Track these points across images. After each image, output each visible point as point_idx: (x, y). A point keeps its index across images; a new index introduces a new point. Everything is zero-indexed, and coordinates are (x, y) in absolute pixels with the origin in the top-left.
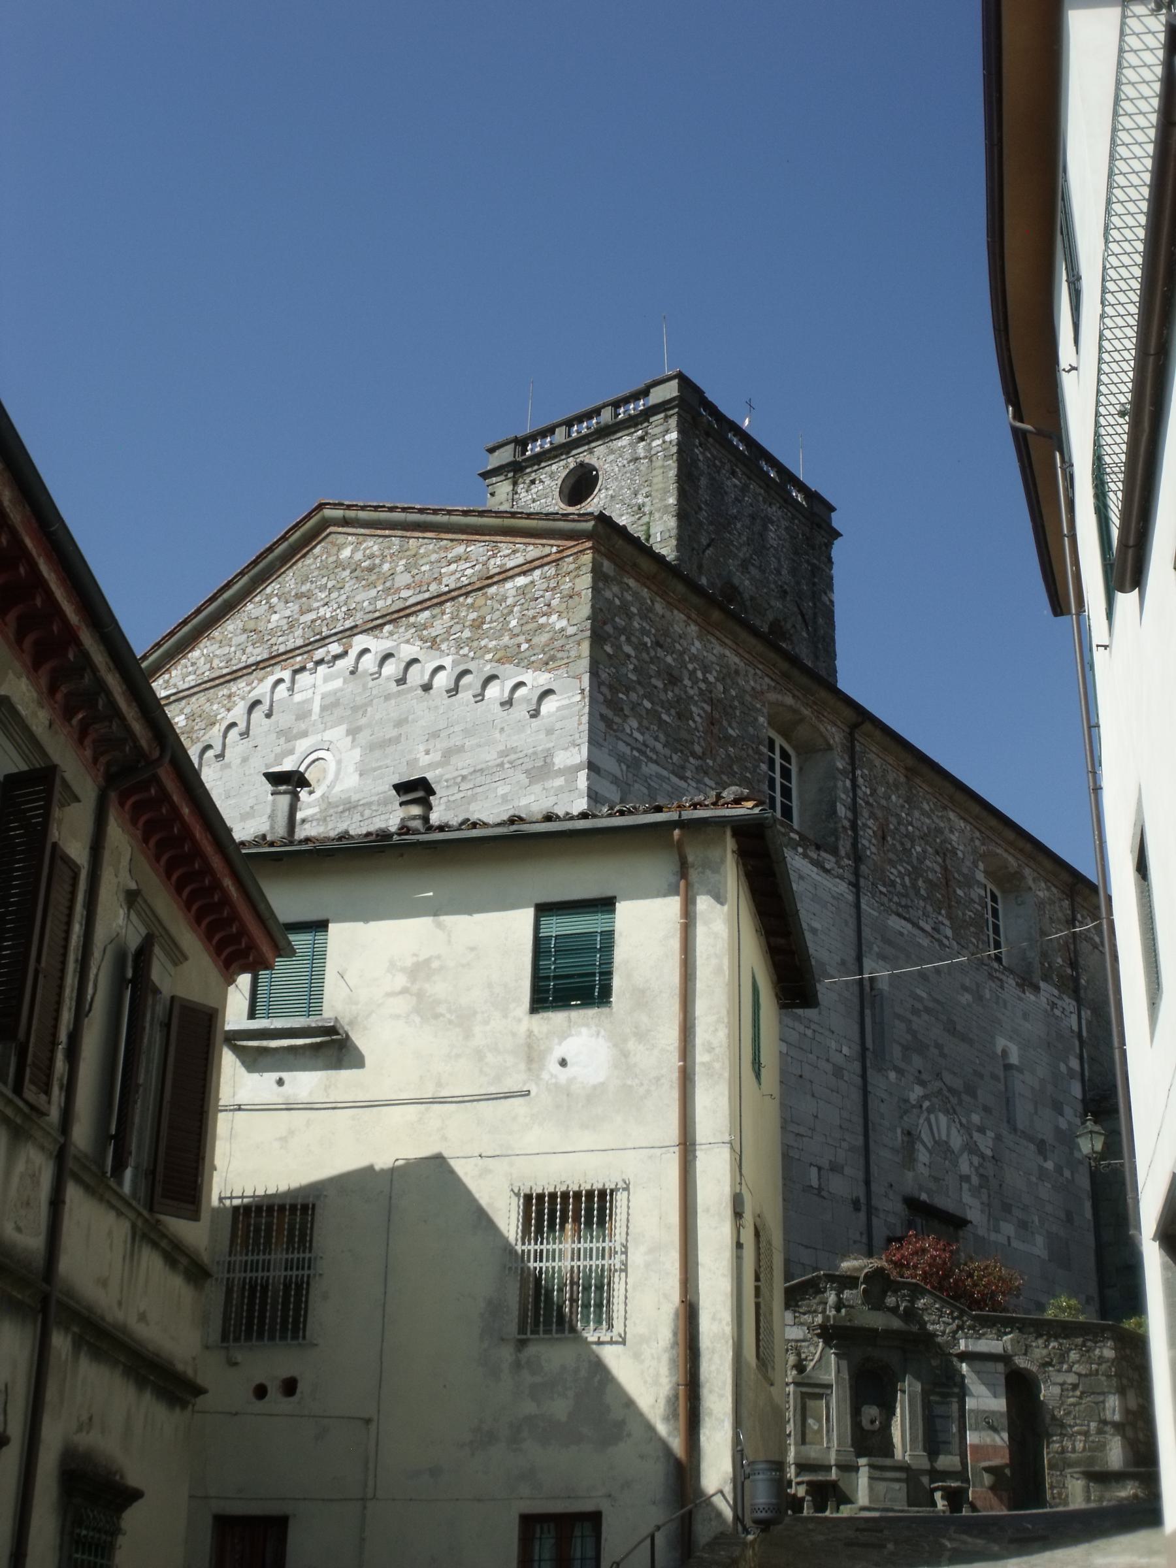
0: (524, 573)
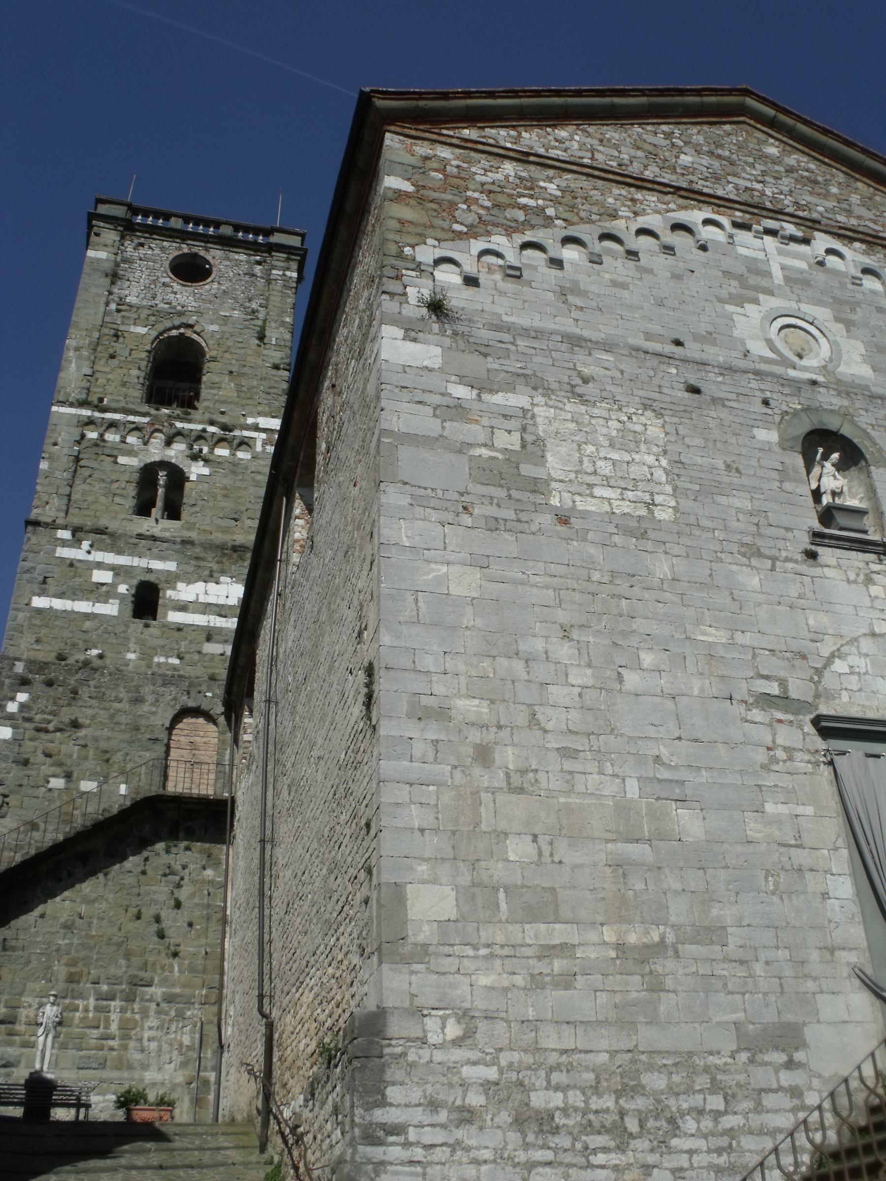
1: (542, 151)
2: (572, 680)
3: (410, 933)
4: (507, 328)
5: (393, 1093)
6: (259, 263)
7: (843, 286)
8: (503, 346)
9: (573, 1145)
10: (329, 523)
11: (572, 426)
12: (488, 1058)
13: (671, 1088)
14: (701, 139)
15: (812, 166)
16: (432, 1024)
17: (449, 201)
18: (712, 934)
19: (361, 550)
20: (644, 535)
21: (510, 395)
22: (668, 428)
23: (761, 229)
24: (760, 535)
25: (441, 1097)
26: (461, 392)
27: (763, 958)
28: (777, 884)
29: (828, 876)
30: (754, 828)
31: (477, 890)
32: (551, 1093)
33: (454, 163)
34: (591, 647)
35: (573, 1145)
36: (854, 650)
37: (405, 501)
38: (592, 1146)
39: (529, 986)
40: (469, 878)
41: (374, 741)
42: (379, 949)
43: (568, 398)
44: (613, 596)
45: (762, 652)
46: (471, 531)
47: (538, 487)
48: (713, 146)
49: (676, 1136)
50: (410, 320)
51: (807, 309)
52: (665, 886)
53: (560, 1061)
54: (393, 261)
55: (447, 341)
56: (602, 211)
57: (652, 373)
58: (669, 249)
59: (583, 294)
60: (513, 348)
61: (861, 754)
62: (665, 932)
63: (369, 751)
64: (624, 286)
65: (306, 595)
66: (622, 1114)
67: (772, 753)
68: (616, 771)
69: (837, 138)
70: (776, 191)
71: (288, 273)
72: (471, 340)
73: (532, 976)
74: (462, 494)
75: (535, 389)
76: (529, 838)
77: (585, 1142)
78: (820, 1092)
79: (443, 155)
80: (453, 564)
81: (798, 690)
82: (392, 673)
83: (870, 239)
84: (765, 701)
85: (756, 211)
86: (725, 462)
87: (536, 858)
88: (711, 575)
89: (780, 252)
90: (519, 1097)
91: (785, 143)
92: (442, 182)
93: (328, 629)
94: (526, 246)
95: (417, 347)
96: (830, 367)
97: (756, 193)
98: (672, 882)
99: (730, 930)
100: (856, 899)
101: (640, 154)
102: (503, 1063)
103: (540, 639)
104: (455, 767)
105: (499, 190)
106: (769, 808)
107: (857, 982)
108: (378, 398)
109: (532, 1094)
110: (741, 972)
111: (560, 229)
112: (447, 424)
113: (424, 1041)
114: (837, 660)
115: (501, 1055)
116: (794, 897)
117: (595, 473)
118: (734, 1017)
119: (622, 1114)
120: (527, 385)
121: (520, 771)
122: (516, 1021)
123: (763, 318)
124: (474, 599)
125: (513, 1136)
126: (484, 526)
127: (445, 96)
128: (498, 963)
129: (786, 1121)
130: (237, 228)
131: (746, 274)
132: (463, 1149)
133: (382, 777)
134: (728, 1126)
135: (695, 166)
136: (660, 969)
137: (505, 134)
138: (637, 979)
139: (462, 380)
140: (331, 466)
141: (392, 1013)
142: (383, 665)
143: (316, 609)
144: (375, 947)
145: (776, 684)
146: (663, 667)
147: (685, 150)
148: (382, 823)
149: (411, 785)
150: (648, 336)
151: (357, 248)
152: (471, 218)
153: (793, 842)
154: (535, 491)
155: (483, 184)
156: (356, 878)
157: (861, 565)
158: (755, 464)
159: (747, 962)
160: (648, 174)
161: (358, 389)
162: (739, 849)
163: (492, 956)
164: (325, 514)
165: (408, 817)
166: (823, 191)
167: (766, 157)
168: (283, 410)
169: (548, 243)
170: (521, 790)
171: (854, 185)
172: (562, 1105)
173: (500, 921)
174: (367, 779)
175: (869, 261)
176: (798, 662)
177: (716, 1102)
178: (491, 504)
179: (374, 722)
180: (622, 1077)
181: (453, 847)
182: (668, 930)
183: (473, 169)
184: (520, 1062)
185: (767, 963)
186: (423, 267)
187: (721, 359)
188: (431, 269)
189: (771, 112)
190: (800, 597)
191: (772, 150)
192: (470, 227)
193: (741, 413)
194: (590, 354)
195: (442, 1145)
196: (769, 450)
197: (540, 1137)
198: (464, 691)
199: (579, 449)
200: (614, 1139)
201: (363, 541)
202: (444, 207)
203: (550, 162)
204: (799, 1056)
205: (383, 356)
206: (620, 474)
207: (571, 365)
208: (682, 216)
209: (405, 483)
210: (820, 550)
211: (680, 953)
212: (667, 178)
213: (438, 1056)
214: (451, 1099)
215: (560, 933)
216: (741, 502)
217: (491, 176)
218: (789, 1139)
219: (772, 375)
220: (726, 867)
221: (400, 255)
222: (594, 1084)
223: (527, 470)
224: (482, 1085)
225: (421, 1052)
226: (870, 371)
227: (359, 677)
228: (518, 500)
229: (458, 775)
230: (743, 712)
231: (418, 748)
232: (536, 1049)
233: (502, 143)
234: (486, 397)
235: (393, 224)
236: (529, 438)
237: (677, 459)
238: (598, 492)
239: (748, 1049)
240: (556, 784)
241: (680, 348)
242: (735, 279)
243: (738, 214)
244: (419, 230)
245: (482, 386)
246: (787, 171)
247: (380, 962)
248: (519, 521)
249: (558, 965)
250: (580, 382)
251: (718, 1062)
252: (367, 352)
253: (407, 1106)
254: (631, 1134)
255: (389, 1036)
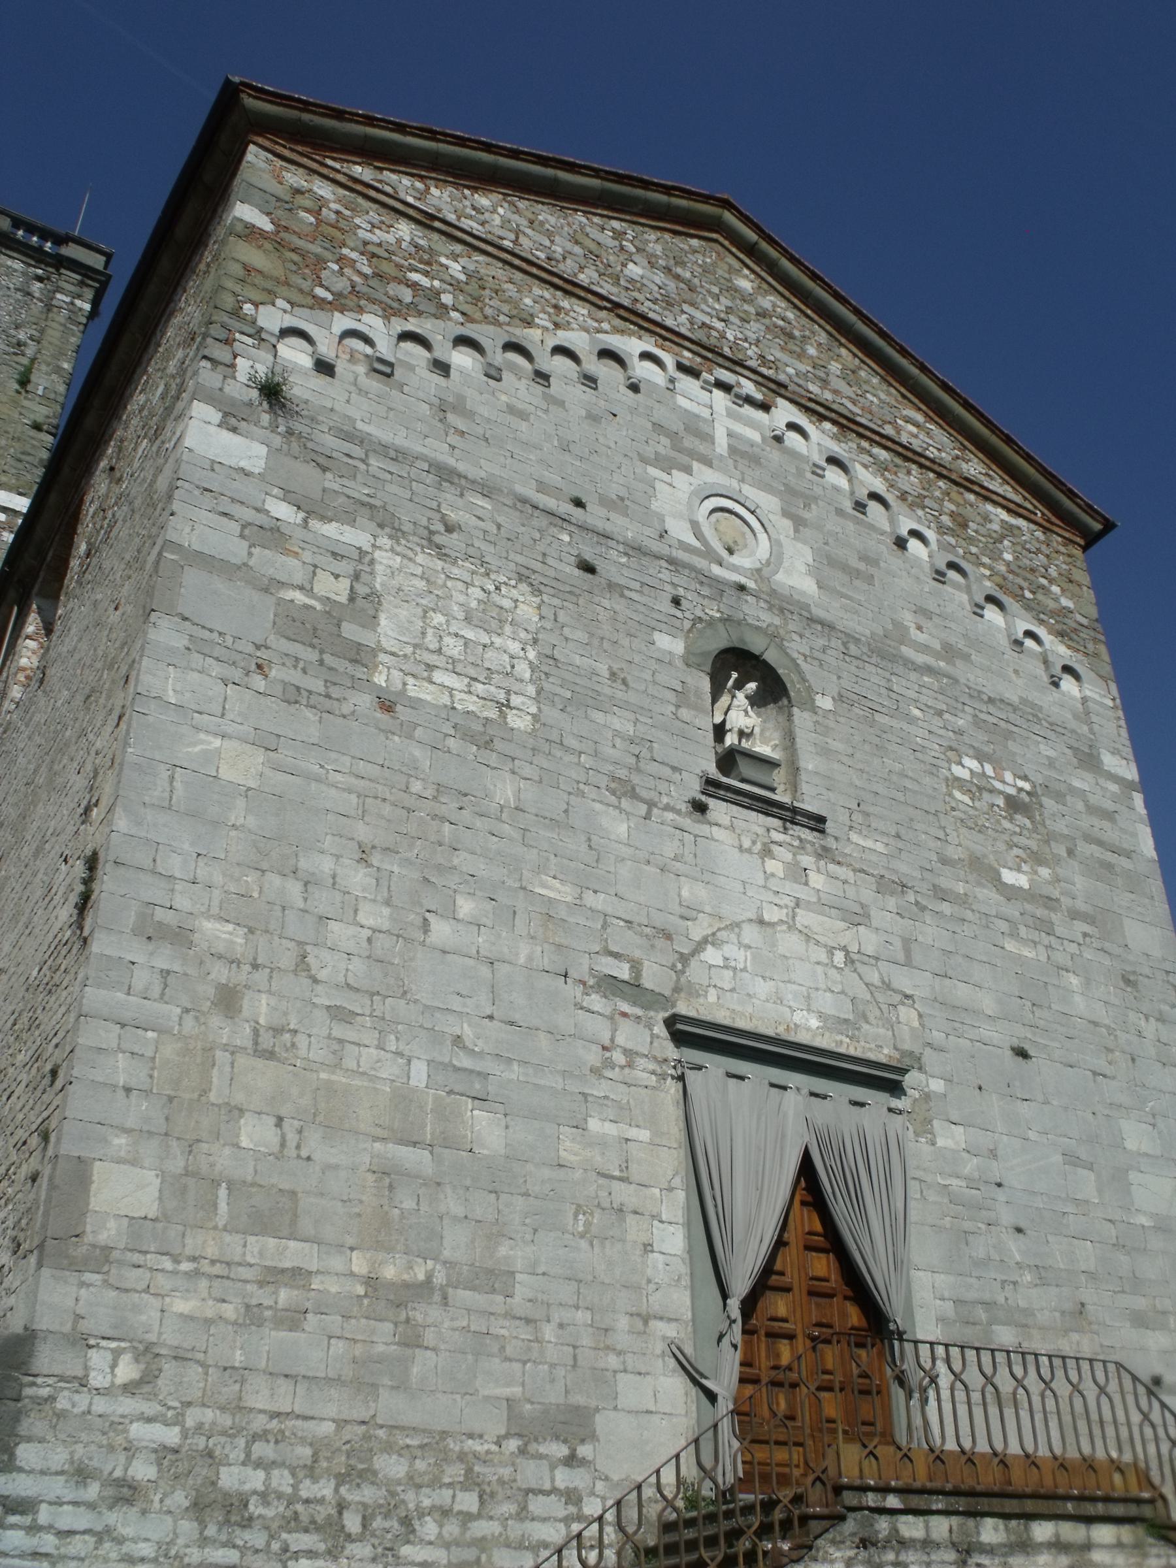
0: (1009, 511)
1: (452, 217)
2: (361, 918)
3: (89, 1228)
4: (360, 439)
5: (26, 1454)
6: (40, 279)
7: (800, 473)
8: (350, 461)
9: (268, 1544)
10: (71, 653)
11: (422, 584)
12: (170, 1414)
13: (411, 1478)
14: (658, 249)
15: (790, 315)
16: (98, 1359)
17: (316, 255)
18: (494, 1279)
19: (109, 697)
20: (488, 744)
21: (346, 528)
22: (545, 611)
23: (712, 379)
24: (638, 770)
25: (95, 1463)
26: (282, 511)
27: (556, 1317)
28: (588, 1224)
29: (656, 1223)
30: (569, 1148)
31: (191, 1182)
32: (249, 1471)
33: (333, 206)
34: (394, 879)
35: (268, 1544)
36: (733, 937)
37: (180, 642)
38: (293, 1548)
39: (241, 1321)
40: (182, 1164)
41: (82, 959)
42: (41, 1246)
43: (423, 547)
44: (435, 817)
45: (616, 921)
46: (262, 699)
47: (361, 655)
48: (672, 262)
49: (408, 1542)
50: (233, 402)
51: (750, 492)
52: (442, 1209)
53: (268, 1427)
54: (225, 318)
55: (277, 441)
56: (515, 312)
57: (538, 536)
58: (590, 380)
59: (470, 415)
60: (363, 467)
61: (721, 1072)
62: (433, 1270)
63: (73, 971)
64: (523, 416)
65: (21, 746)
66: (341, 1507)
67: (608, 1054)
68: (401, 1048)
69: (827, 287)
70: (740, 336)
71: (78, 302)
72: (310, 445)
73: (248, 1307)
74: (258, 647)
75: (381, 526)
76: (272, 1121)
77: (285, 1542)
78: (604, 1499)
79: (321, 192)
80: (230, 737)
81: (654, 977)
82: (122, 870)
83: (845, 422)
84: (610, 985)
85: (710, 355)
86: (610, 668)
87: (276, 1149)
88: (566, 811)
89: (730, 414)
90: (204, 1472)
91: (763, 279)
92: (311, 229)
93: (44, 796)
94: (406, 336)
95: (236, 439)
96: (765, 573)
97: (714, 333)
98: (452, 1204)
99: (519, 1277)
100: (686, 1256)
101: (577, 250)
102: (190, 1423)
103: (329, 858)
104: (187, 1011)
105: (386, 255)
106: (594, 1125)
107: (672, 1362)
108: (170, 497)
109: (223, 1469)
110: (525, 1333)
111: (454, 325)
112: (256, 551)
113: (83, 1382)
114: (709, 947)
115: (190, 1412)
116: (608, 1243)
117: (439, 651)
118: (507, 1391)
119: (341, 1507)
120: (371, 519)
121: (274, 1029)
122: (216, 1366)
123: (692, 493)
124: (249, 789)
125: (187, 1527)
126: (280, 694)
127: (339, 115)
128: (203, 1284)
129: (554, 1534)
130: (17, 223)
131: (682, 433)
132: (113, 1540)
133: (85, 1010)
134: (479, 1535)
135: (645, 281)
136: (419, 1317)
137: (409, 184)
138: (388, 1327)
139: (288, 496)
140: (88, 577)
141: (45, 1339)
142: (111, 858)
143: (32, 767)
144: (36, 1242)
145: (626, 966)
146: (484, 920)
147: (636, 258)
148: (75, 1073)
149: (123, 1026)
150: (542, 487)
151: (180, 290)
152: (341, 285)
153: (617, 1173)
154: (356, 661)
155: (366, 243)
156: (25, 1143)
157: (761, 831)
158: (649, 678)
159: (535, 1321)
160: (583, 278)
161: (144, 480)
162: (547, 1173)
163: (197, 1273)
164: (67, 640)
165: (112, 1067)
166: (798, 350)
167: (736, 291)
168: (35, 487)
169: (436, 339)
170: (270, 1055)
171: (836, 350)
172: (260, 1487)
173: (215, 1228)
174: (63, 1009)
175: (838, 449)
176: (660, 943)
177: (468, 1501)
178: (295, 667)
179: (85, 934)
180: (348, 1457)
181: (167, 1119)
182: (438, 1267)
183: (357, 221)
184: (214, 1423)
185: (561, 1326)
186: (264, 336)
187: (630, 535)
188: (273, 340)
189: (752, 236)
190: (676, 858)
191: (745, 283)
192: (338, 295)
193: (642, 609)
194: (462, 495)
195: (84, 1532)
196: (670, 663)
197: (225, 1530)
198: (215, 910)
199: (425, 617)
200: (324, 1541)
201: (114, 684)
202: (309, 261)
203: (459, 234)
204: (584, 1451)
205: (188, 442)
206: (471, 659)
207: (434, 505)
208: (616, 342)
209: (185, 619)
210: (712, 803)
211: (450, 1300)
212: (606, 288)
213: (101, 1405)
214: (109, 1468)
215: (295, 1253)
216: (621, 723)
217: (379, 236)
218: (555, 1557)
219: (692, 568)
220: (526, 1194)
221: (236, 313)
222: (309, 1463)
223: (350, 631)
224: (155, 1451)
225: (76, 1397)
226: (815, 587)
227: (76, 869)
228: (331, 669)
229: (189, 1021)
230: (579, 995)
231: (141, 978)
232: (238, 1407)
233: (402, 195)
234: (314, 524)
235: (236, 269)
236: (362, 590)
237: (549, 653)
238: (438, 676)
239: (519, 1435)
240: (318, 1053)
241: (580, 510)
242: (667, 436)
243: (687, 354)
244: (269, 285)
245: (312, 509)
246: (758, 314)
247: (40, 1265)
248: (328, 696)
249: (285, 1296)
250: (442, 529)
251: (478, 1448)
252: (167, 433)
253: (43, 1473)
254: (349, 1535)
255: (34, 1371)
